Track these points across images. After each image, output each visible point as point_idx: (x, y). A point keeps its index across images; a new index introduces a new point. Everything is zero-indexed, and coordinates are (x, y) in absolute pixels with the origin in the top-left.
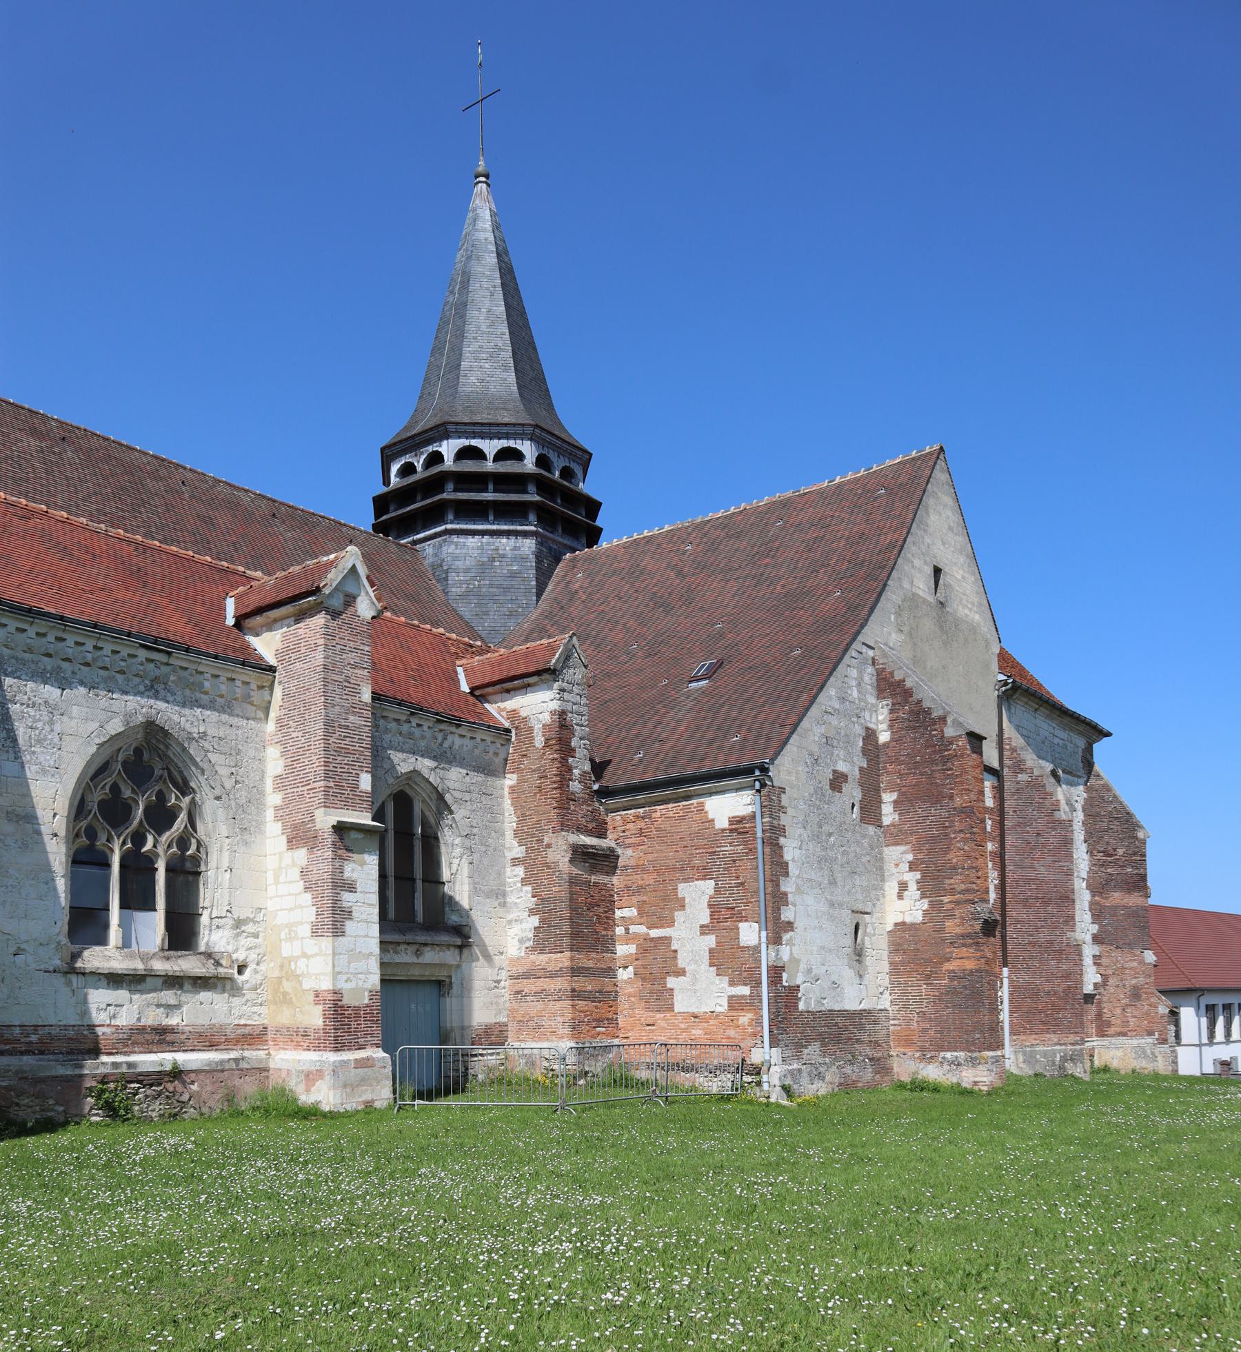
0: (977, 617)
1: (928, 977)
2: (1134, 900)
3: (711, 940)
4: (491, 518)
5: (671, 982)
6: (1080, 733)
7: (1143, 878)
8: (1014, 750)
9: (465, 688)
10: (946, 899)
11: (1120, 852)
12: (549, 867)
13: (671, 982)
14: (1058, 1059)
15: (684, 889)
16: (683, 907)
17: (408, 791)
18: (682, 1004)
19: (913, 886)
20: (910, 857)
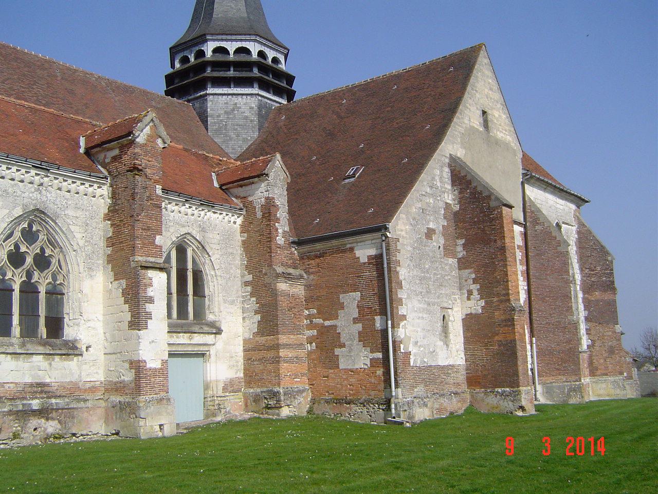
0: (508, 137)
1: (486, 345)
2: (607, 296)
3: (359, 327)
4: (232, 86)
5: (337, 351)
6: (572, 202)
7: (613, 282)
8: (532, 212)
9: (216, 184)
10: (495, 299)
11: (599, 268)
12: (266, 287)
13: (337, 351)
14: (566, 390)
15: (343, 298)
16: (343, 308)
17: (184, 244)
18: (342, 366)
19: (475, 293)
20: (473, 276)
